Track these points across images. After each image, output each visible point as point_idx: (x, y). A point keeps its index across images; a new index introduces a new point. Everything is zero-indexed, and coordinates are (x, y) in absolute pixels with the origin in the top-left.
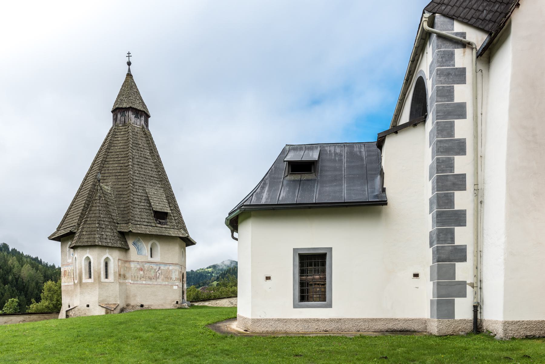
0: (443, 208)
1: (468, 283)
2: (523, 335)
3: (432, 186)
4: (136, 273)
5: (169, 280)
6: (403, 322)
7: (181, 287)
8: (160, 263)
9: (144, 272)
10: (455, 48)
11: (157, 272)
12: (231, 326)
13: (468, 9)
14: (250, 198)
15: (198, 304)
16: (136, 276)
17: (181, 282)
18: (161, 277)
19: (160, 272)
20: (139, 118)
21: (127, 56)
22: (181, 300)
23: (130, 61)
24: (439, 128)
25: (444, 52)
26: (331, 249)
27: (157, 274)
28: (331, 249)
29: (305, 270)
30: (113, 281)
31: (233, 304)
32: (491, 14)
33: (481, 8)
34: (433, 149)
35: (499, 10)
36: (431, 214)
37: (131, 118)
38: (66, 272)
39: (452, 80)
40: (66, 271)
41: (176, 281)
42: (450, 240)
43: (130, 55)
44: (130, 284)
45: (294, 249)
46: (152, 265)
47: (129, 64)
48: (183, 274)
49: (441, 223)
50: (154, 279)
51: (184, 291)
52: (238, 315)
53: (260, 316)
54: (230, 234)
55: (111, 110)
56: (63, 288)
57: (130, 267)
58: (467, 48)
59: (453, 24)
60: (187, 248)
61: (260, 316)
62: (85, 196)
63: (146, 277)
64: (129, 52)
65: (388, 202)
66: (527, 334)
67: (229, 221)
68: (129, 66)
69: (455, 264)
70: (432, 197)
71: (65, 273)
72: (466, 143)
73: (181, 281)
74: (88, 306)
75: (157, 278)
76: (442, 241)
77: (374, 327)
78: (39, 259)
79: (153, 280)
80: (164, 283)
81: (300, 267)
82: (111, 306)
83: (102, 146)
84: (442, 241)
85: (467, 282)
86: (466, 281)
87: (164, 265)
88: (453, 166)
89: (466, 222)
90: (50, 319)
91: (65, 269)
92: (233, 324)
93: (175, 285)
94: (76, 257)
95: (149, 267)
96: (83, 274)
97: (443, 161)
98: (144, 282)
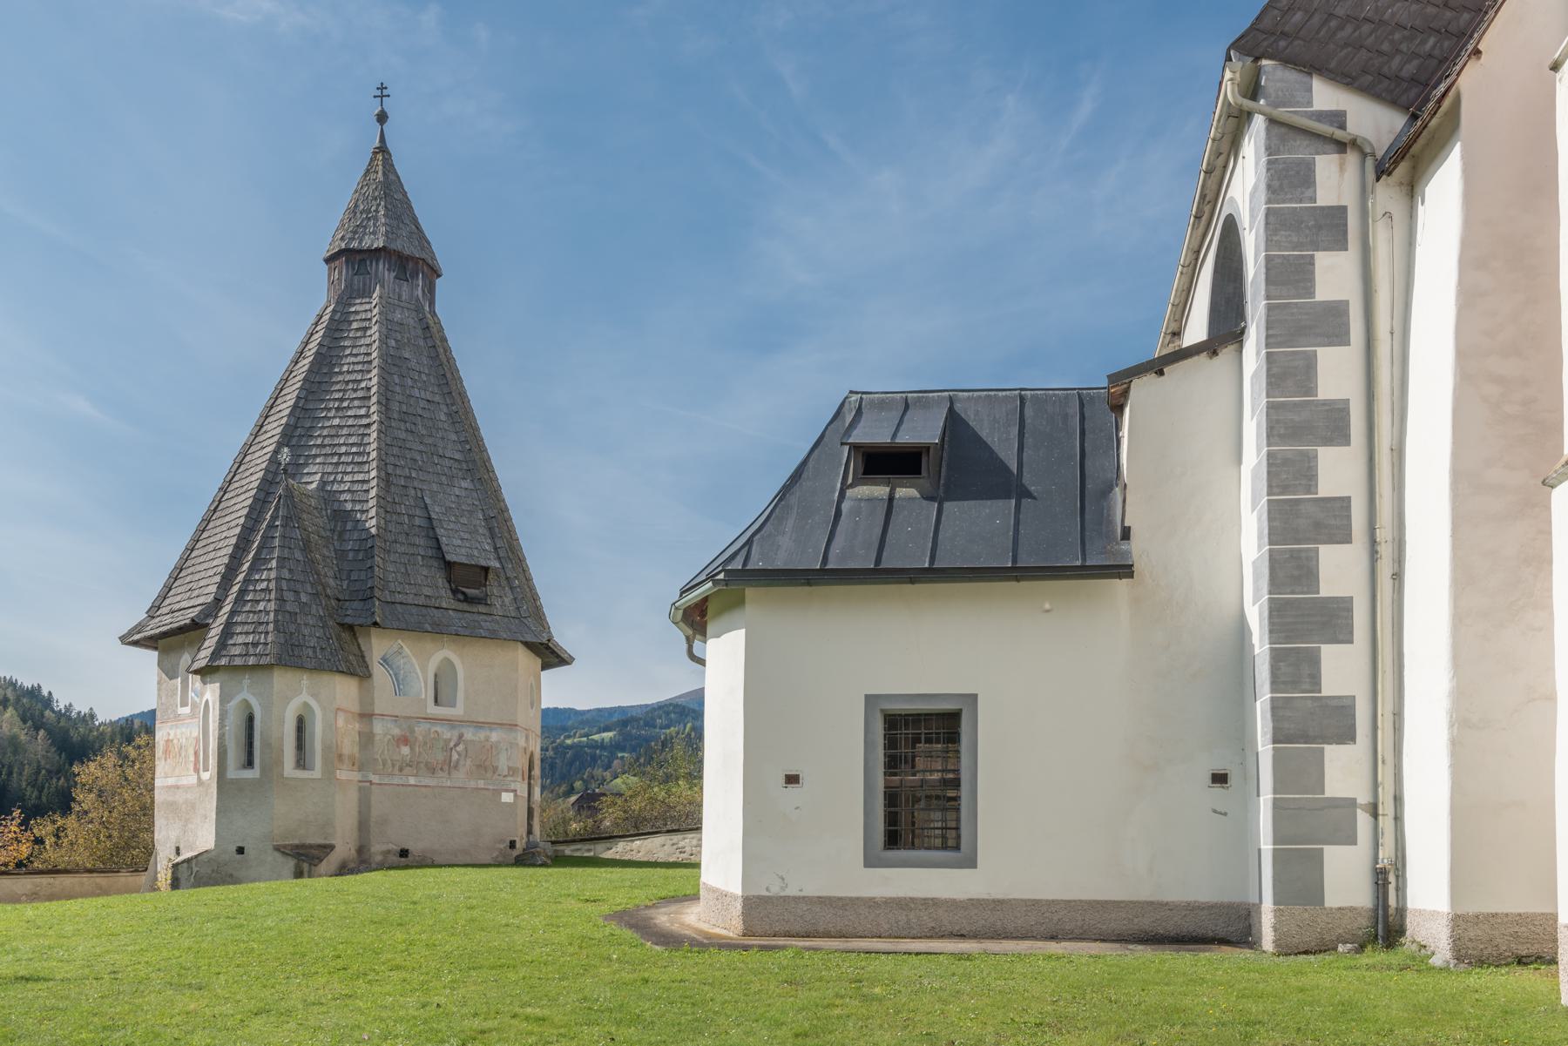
0: (1288, 591)
1: (1361, 805)
2: (1507, 954)
3: (1259, 529)
4: (388, 750)
5: (489, 775)
6: (1183, 914)
7: (526, 795)
8: (461, 722)
9: (412, 749)
10: (1318, 154)
11: (451, 749)
12: (683, 916)
13: (1350, 49)
14: (743, 551)
15: (573, 851)
16: (389, 762)
17: (526, 781)
18: (465, 765)
19: (461, 748)
20: (408, 281)
21: (375, 97)
22: (525, 836)
24: (1275, 370)
25: (1284, 163)
26: (974, 697)
27: (451, 756)
28: (974, 697)
29: (901, 756)
30: (320, 777)
31: (684, 852)
32: (1415, 63)
33: (1385, 47)
34: (1258, 425)
35: (1437, 52)
36: (1257, 606)
37: (384, 280)
38: (171, 744)
39: (1309, 239)
40: (172, 741)
41: (509, 778)
42: (1308, 680)
44: (368, 784)
45: (868, 697)
46: (438, 729)
48: (532, 755)
49: (1283, 634)
50: (441, 769)
51: (533, 809)
52: (704, 883)
53: (767, 889)
54: (685, 646)
56: (159, 796)
57: (372, 732)
58: (1348, 150)
59: (1310, 90)
60: (546, 675)
61: (767, 889)
62: (239, 514)
63: (418, 763)
64: (382, 84)
65: (1135, 569)
66: (1519, 952)
67: (681, 612)
68: (382, 125)
69: (1323, 748)
70: (1258, 558)
71: (167, 746)
72: (1348, 413)
73: (526, 776)
74: (241, 851)
75: (450, 766)
76: (1284, 683)
77: (1099, 925)
78: (45, 693)
79: (441, 774)
80: (472, 784)
81: (885, 768)
82: (313, 851)
83: (292, 362)
84: (1284, 683)
85: (1358, 801)
86: (1355, 799)
87: (476, 727)
88: (1313, 476)
89: (1351, 633)
91: (169, 734)
92: (689, 911)
93: (507, 791)
94: (207, 701)
95: (430, 734)
96: (229, 751)
97: (1286, 462)
98: (412, 781)
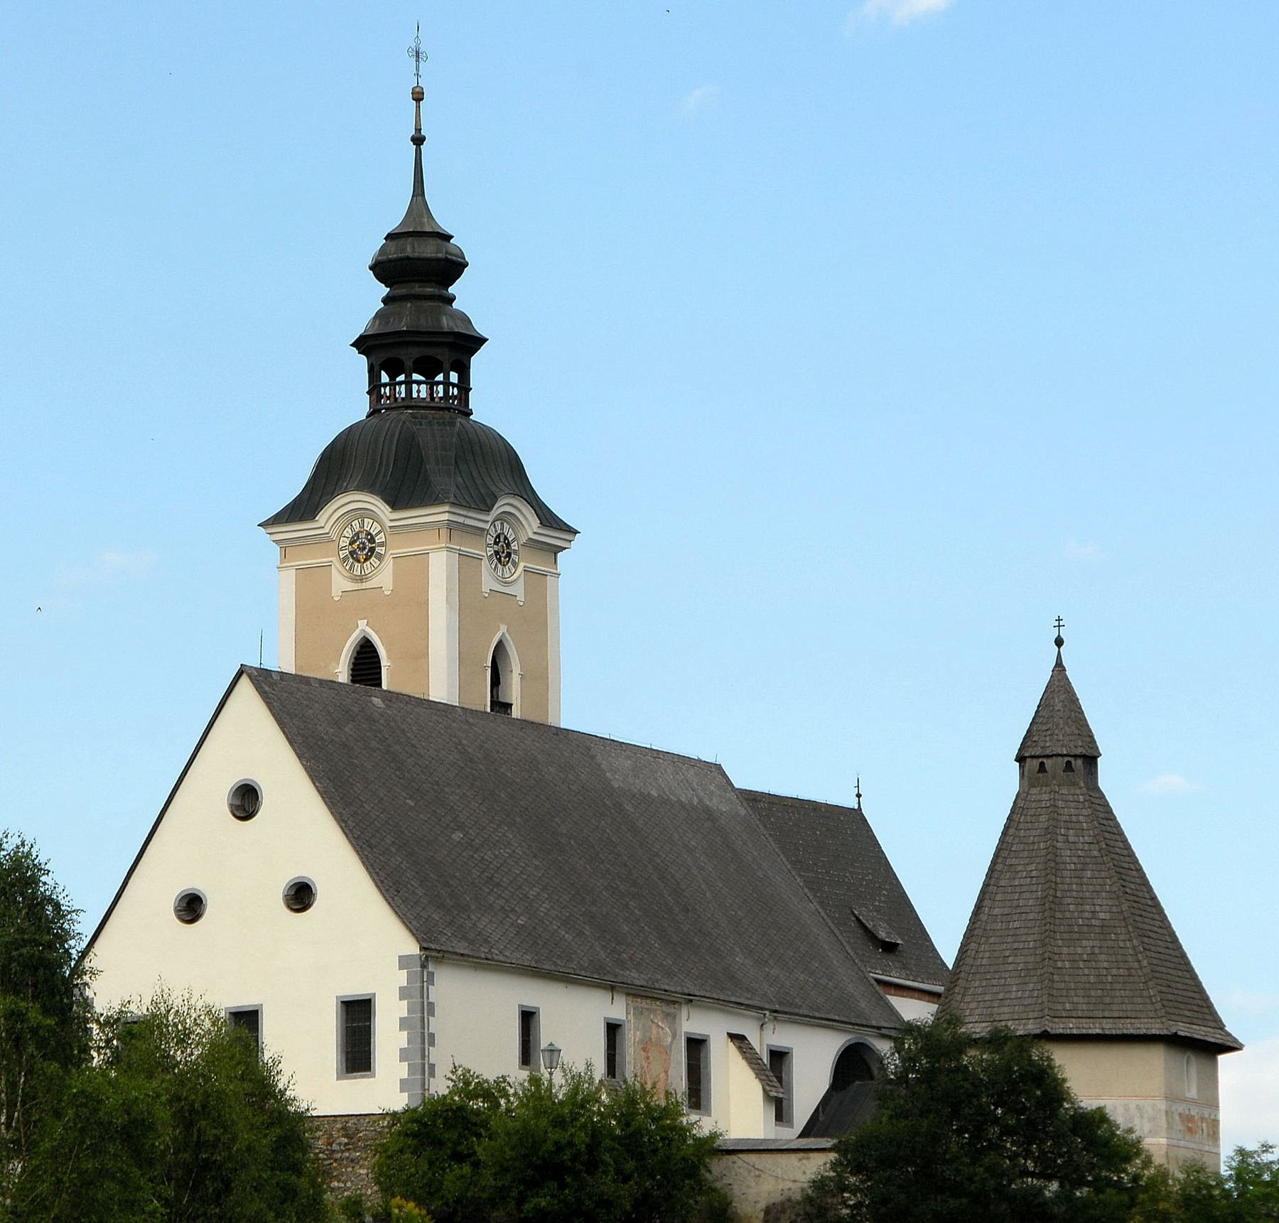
23: (444, 218)
43: (1061, 623)
47: (1059, 642)
55: (370, 262)
68: (1059, 648)
90: (700, 1090)
